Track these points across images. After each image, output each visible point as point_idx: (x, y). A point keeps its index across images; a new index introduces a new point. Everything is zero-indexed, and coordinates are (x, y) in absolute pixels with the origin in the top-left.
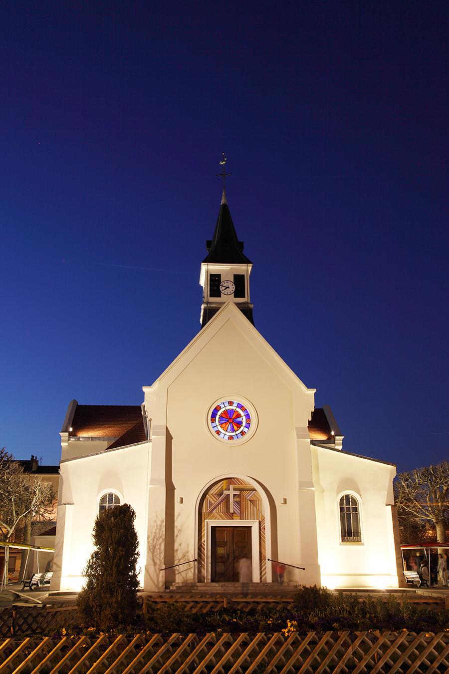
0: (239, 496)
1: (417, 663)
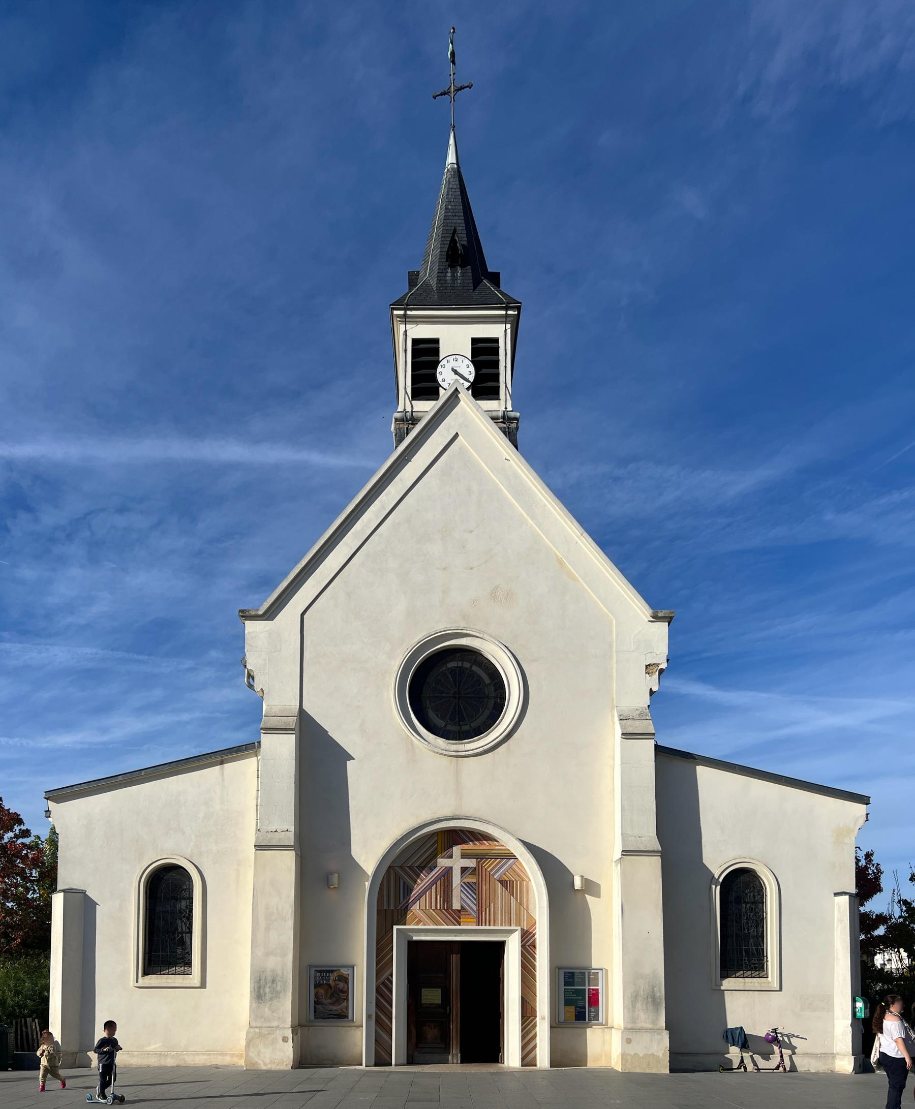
0: (474, 871)
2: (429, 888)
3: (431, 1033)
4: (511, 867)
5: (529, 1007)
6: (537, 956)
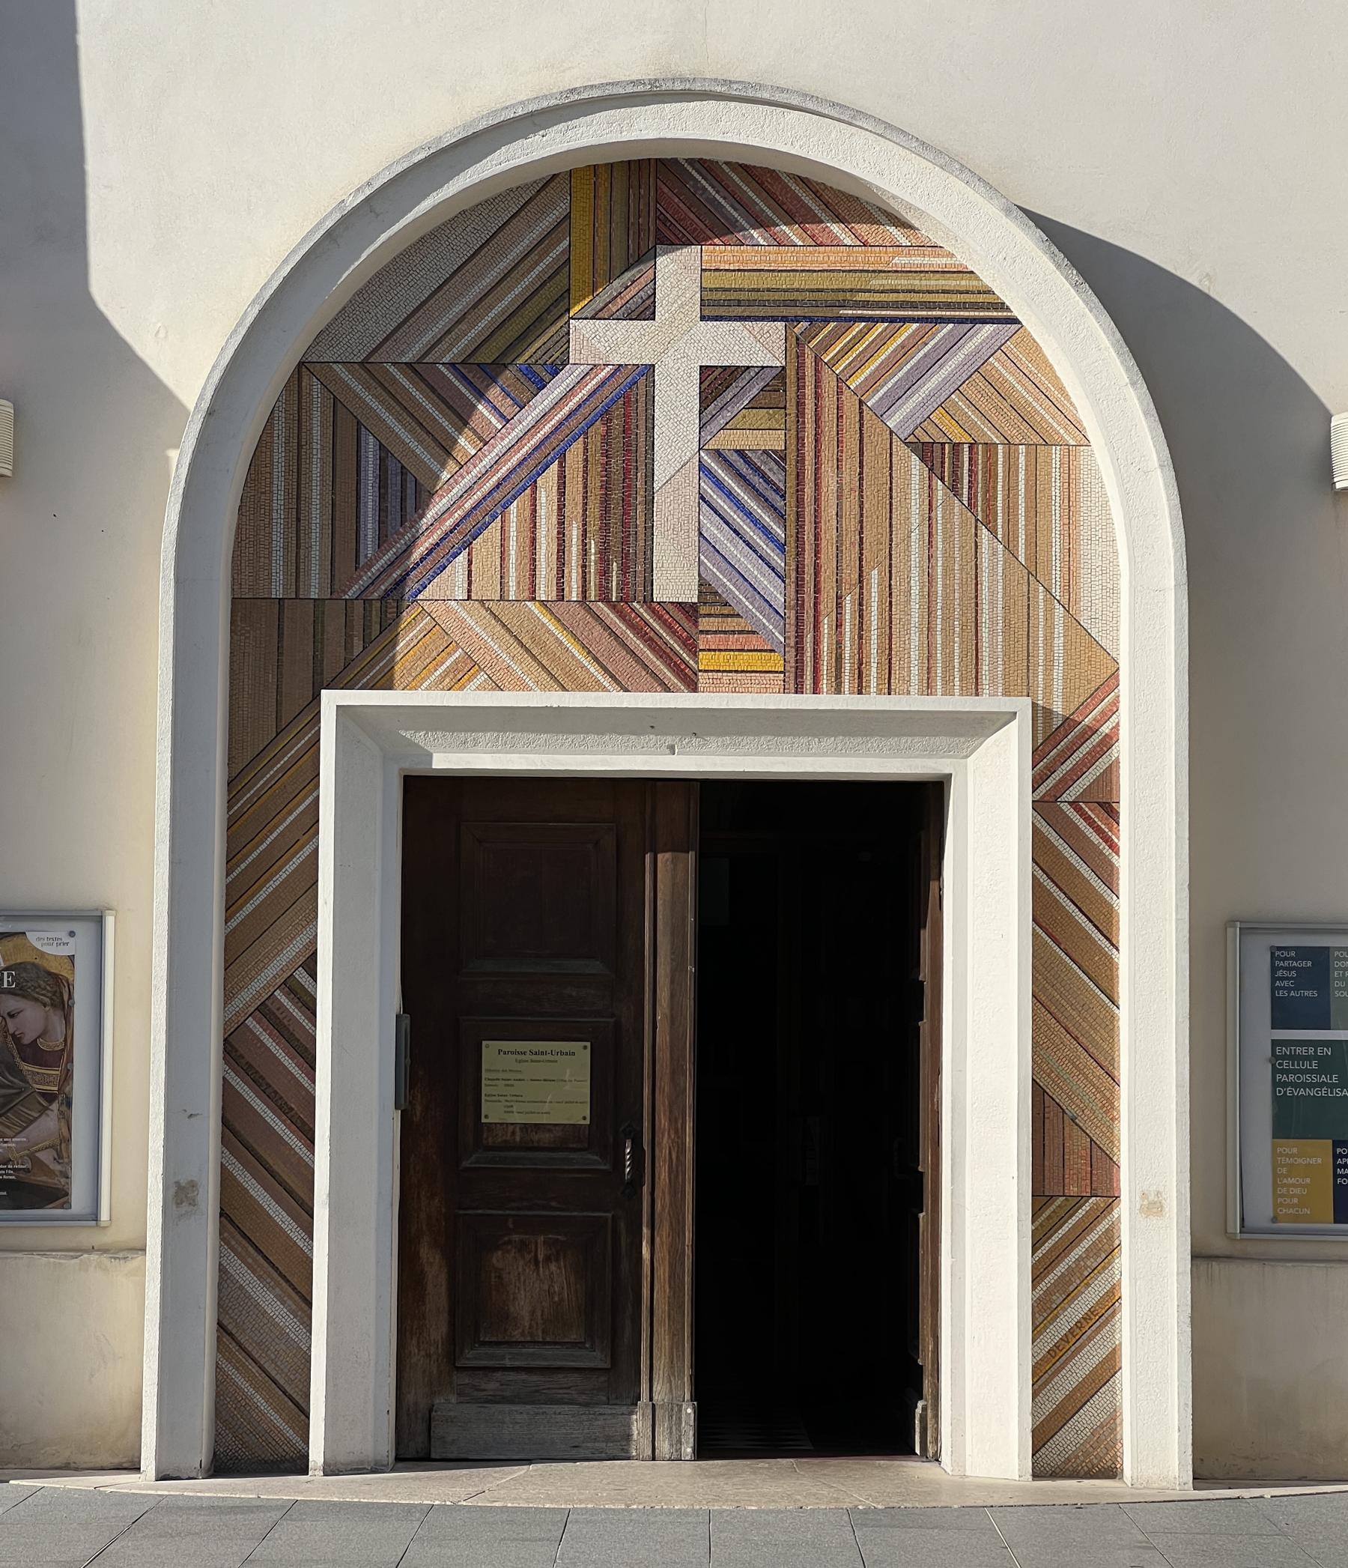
0: (776, 389)
1: (539, 1141)
2: (522, 482)
3: (534, 1285)
4: (978, 369)
5: (1077, 1145)
6: (1123, 862)
